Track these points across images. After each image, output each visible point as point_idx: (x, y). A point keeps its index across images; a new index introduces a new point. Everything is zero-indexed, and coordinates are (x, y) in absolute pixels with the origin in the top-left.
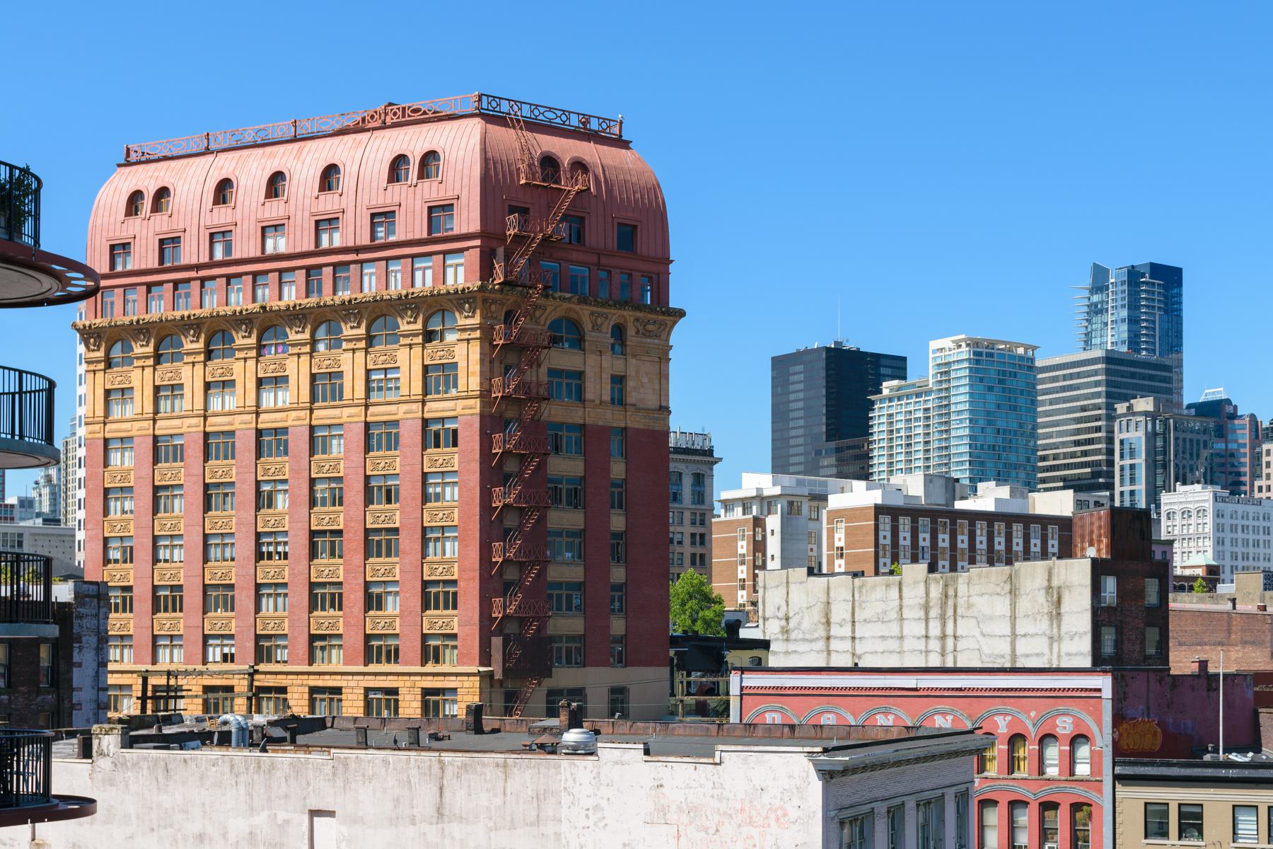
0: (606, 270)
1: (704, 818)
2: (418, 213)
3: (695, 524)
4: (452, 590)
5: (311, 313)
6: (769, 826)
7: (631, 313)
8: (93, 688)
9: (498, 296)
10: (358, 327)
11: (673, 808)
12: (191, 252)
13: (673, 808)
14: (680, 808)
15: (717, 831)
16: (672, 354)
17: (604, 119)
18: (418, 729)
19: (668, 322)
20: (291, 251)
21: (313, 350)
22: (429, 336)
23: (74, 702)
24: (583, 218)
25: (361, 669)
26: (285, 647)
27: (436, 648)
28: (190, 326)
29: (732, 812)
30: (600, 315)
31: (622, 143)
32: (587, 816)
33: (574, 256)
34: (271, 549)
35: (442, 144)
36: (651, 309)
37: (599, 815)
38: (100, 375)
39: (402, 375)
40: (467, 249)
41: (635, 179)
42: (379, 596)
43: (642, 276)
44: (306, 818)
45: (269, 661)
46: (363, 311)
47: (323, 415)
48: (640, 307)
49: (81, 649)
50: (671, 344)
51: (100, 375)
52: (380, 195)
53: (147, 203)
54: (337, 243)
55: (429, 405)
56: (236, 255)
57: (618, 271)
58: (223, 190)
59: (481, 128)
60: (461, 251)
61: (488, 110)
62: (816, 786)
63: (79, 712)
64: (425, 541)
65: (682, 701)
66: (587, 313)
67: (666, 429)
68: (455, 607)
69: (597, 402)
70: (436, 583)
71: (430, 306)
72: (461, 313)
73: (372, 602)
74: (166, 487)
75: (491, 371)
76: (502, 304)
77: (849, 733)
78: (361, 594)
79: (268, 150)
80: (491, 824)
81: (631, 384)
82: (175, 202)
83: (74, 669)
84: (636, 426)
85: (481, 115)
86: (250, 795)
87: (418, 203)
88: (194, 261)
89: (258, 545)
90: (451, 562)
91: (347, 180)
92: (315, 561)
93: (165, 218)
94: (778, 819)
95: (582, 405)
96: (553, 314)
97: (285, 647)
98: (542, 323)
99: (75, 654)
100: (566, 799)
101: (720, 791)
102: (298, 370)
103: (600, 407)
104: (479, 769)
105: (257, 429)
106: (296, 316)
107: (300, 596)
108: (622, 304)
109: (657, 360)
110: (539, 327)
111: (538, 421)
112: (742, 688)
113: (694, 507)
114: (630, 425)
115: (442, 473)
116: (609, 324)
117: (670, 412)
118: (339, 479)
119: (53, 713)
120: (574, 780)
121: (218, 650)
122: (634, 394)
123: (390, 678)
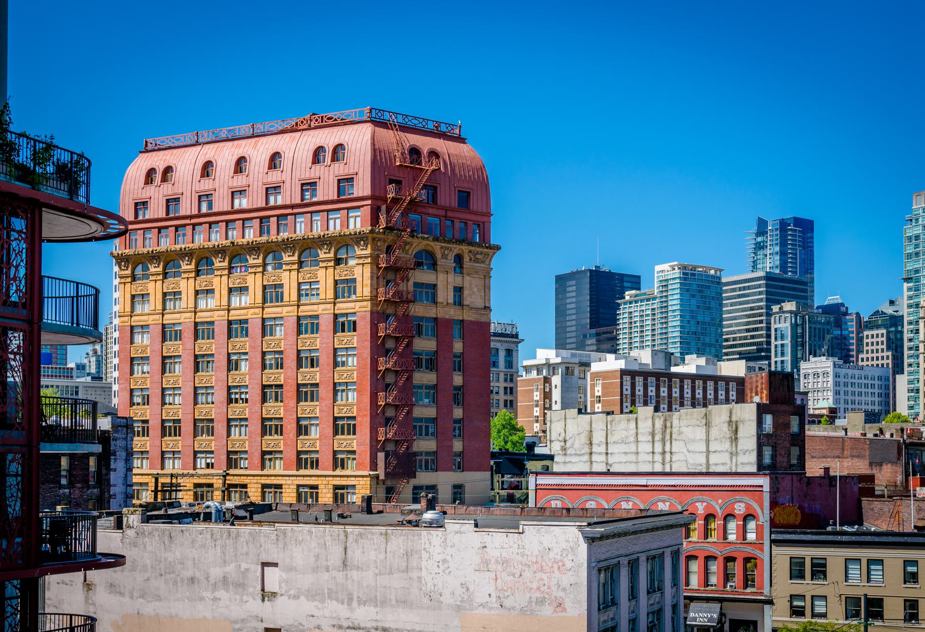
1: (512, 568)
2: (331, 183)
4: (352, 422)
6: (553, 572)
9: (382, 236)
10: (293, 255)
11: (493, 561)
12: (186, 207)
13: (493, 561)
14: (497, 561)
15: (521, 575)
16: (492, 273)
18: (330, 511)
20: (250, 207)
21: (264, 270)
22: (338, 261)
25: (295, 472)
26: (246, 459)
27: (342, 460)
28: (186, 255)
29: (530, 563)
30: (447, 248)
31: (460, 140)
32: (438, 566)
33: (431, 211)
34: (237, 396)
35: (346, 139)
36: (479, 245)
37: (446, 565)
38: (128, 285)
39: (321, 286)
40: (363, 206)
41: (469, 163)
42: (306, 427)
44: (259, 567)
45: (236, 467)
46: (296, 245)
47: (270, 312)
48: (471, 244)
51: (128, 285)
52: (308, 172)
53: (158, 177)
55: (338, 305)
57: (458, 221)
58: (207, 169)
60: (358, 207)
62: (583, 547)
64: (335, 392)
65: (498, 493)
66: (438, 247)
67: (488, 321)
68: (354, 434)
69: (445, 304)
72: (358, 247)
73: (302, 430)
74: (170, 357)
75: (378, 283)
76: (384, 241)
77: (604, 514)
78: (294, 425)
79: (236, 142)
80: (377, 571)
81: (466, 292)
82: (176, 175)
85: (371, 121)
86: (224, 553)
88: (188, 213)
89: (229, 394)
90: (352, 405)
91: (286, 162)
92: (265, 404)
94: (559, 568)
97: (246, 459)
99: (112, 463)
100: (425, 555)
101: (522, 550)
102: (254, 282)
104: (369, 536)
105: (228, 320)
106: (253, 248)
108: (461, 242)
109: (483, 277)
112: (536, 485)
114: (466, 318)
115: (346, 348)
118: (281, 352)
120: (430, 543)
121: (203, 460)
122: (468, 298)
123: (313, 478)
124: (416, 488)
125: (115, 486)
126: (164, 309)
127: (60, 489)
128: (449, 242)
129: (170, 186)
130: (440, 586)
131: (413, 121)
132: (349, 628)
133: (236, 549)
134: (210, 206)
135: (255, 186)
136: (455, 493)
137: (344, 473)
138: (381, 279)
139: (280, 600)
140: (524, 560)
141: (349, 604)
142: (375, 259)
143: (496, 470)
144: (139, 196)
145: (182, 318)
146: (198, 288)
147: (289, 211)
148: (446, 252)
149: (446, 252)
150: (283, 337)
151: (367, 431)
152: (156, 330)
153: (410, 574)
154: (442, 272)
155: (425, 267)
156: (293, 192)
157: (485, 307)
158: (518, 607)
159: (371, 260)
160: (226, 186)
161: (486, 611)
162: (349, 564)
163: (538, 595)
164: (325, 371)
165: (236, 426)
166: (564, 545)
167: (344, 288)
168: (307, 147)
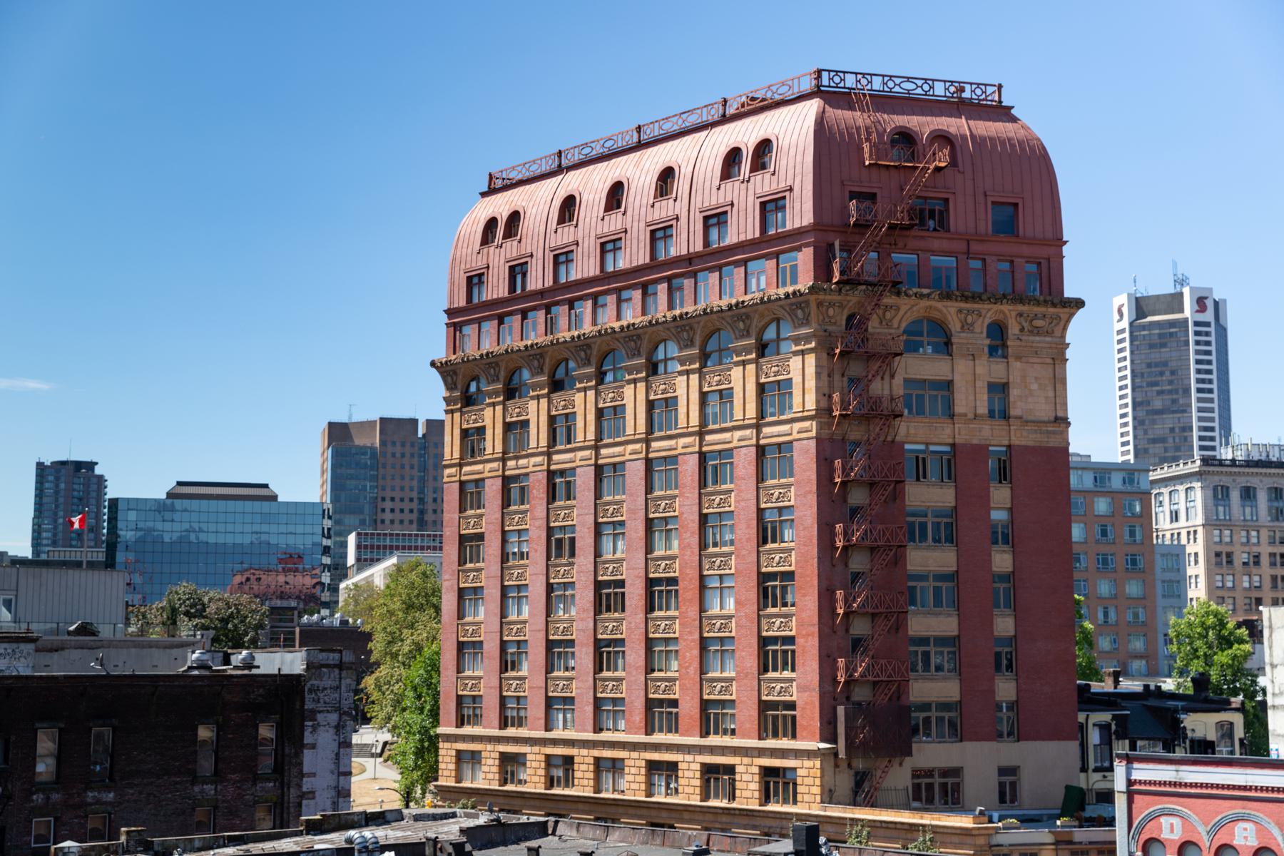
0: (979, 259)
3: (1274, 543)
5: (645, 333)
7: (1011, 308)
8: (332, 772)
9: (836, 298)
12: (537, 279)
16: (1069, 353)
17: (978, 84)
19: (1062, 316)
23: (304, 789)
24: (947, 200)
30: (970, 312)
33: (936, 244)
35: (776, 132)
43: (1027, 262)
49: (314, 729)
50: (1067, 341)
51: (457, 415)
52: (710, 194)
53: (500, 231)
58: (569, 207)
59: (819, 107)
61: (829, 86)
63: (312, 802)
66: (953, 311)
67: (1063, 445)
69: (971, 416)
71: (762, 316)
75: (831, 385)
76: (842, 306)
81: (1014, 392)
82: (526, 226)
83: (305, 751)
85: (817, 92)
87: (751, 199)
91: (681, 185)
93: (515, 243)
95: (950, 421)
96: (909, 314)
98: (896, 325)
99: (307, 734)
103: (975, 422)
109: (1051, 361)
110: (893, 331)
111: (893, 441)
112: (1130, 783)
113: (1271, 524)
114: (1016, 441)
116: (983, 322)
117: (1069, 424)
119: (275, 804)
122: (1019, 404)
124: (917, 774)
125: (314, 775)
127: (193, 784)
128: (976, 297)
131: (903, 85)
135: (635, 229)
143: (1116, 732)
144: (474, 265)
148: (970, 319)
149: (970, 319)
151: (815, 665)
152: (494, 487)
155: (929, 349)
156: (691, 234)
157: (1057, 419)
159: (818, 344)
160: (593, 235)
164: (744, 552)
168: (715, 152)
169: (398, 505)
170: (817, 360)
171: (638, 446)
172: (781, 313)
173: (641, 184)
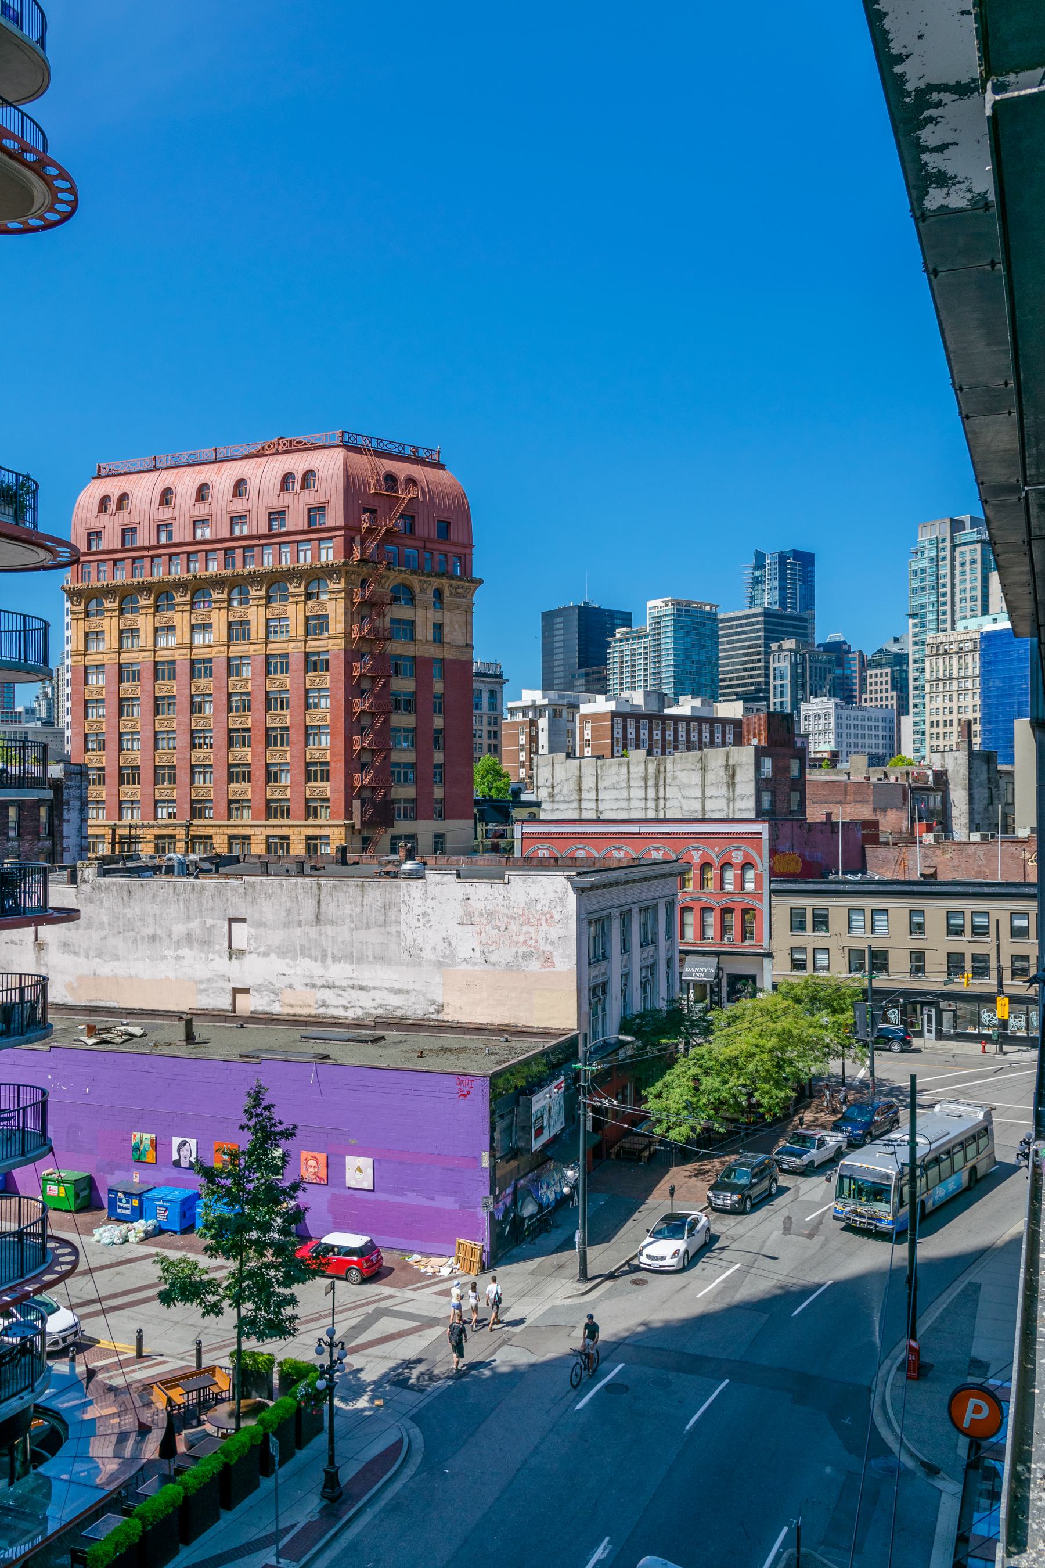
4: (325, 768)
9: (356, 569)
11: (477, 914)
13: (477, 914)
14: (481, 914)
16: (474, 609)
20: (214, 537)
21: (230, 605)
22: (309, 596)
25: (264, 822)
27: (315, 808)
28: (144, 589)
30: (426, 582)
31: (439, 466)
33: (408, 542)
34: (201, 741)
36: (460, 579)
38: (81, 622)
39: (291, 623)
40: (335, 537)
41: (449, 490)
42: (276, 773)
44: (226, 923)
45: (200, 817)
47: (236, 650)
48: (452, 577)
49: (69, 810)
51: (81, 622)
53: (113, 505)
54: (245, 532)
55: (309, 643)
56: (175, 540)
58: (166, 496)
60: (331, 538)
62: (572, 898)
68: (328, 780)
70: (315, 764)
71: (310, 576)
74: (128, 699)
76: (359, 575)
77: (594, 863)
78: (263, 771)
79: (197, 468)
81: (446, 629)
84: (451, 657)
85: (343, 446)
86: (188, 908)
87: (301, 505)
88: (146, 544)
89: (192, 738)
90: (325, 750)
91: (252, 490)
94: (547, 920)
97: (211, 808)
102: (219, 619)
106: (217, 582)
107: (222, 773)
108: (441, 575)
114: (447, 656)
121: (165, 810)
126: (121, 647)
128: (428, 575)
129: (126, 514)
130: (420, 941)
132: (323, 986)
133: (200, 903)
134: (170, 536)
136: (436, 843)
137: (318, 822)
138: (355, 615)
139: (248, 959)
140: (510, 912)
141: (323, 961)
142: (349, 594)
145: (139, 655)
146: (157, 625)
147: (256, 542)
150: (249, 677)
153: (388, 929)
154: (421, 607)
157: (467, 645)
158: (504, 962)
160: (187, 515)
161: (469, 967)
162: (322, 918)
163: (525, 949)
165: (200, 773)
166: (552, 896)
167: (315, 624)
168: (274, 473)
169: (884, 695)
170: (345, 604)
171: (222, 649)
172: (321, 575)
173: (222, 486)
